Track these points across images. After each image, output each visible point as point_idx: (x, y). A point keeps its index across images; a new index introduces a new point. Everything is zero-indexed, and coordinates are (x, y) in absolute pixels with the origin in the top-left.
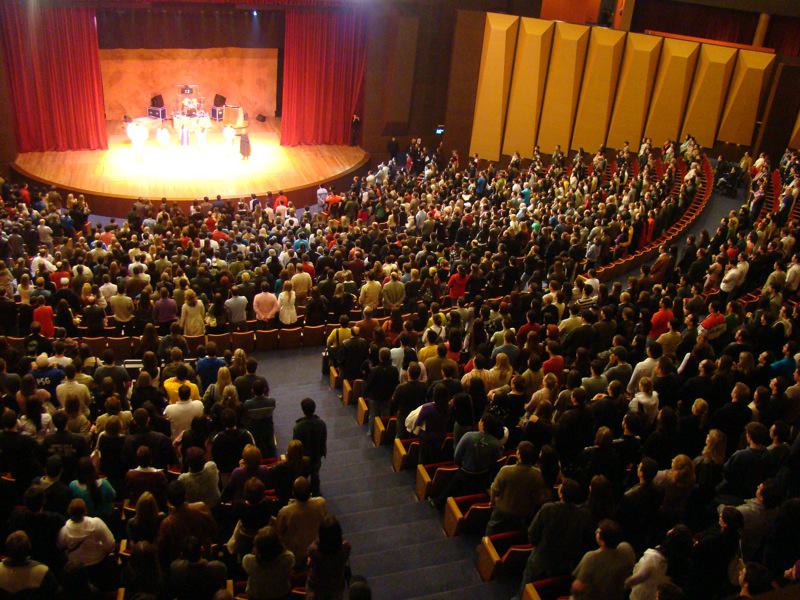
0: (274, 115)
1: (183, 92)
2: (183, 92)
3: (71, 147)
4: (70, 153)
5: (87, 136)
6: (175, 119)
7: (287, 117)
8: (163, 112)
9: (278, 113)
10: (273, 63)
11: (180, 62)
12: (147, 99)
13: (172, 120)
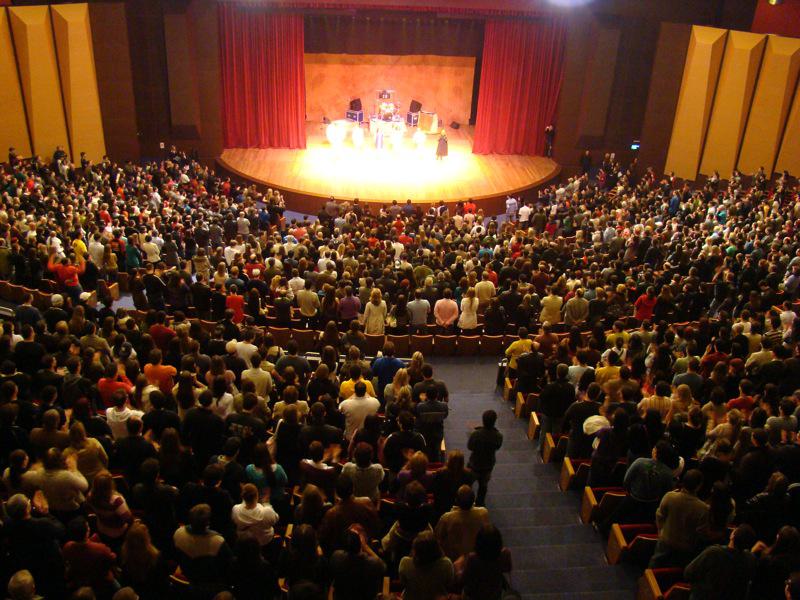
0: (467, 122)
1: (381, 97)
2: (381, 97)
3: (272, 145)
4: (270, 151)
5: (284, 129)
6: (371, 122)
7: (481, 125)
8: (361, 115)
9: (472, 121)
10: (470, 72)
11: (380, 68)
12: (346, 102)
13: (368, 123)
